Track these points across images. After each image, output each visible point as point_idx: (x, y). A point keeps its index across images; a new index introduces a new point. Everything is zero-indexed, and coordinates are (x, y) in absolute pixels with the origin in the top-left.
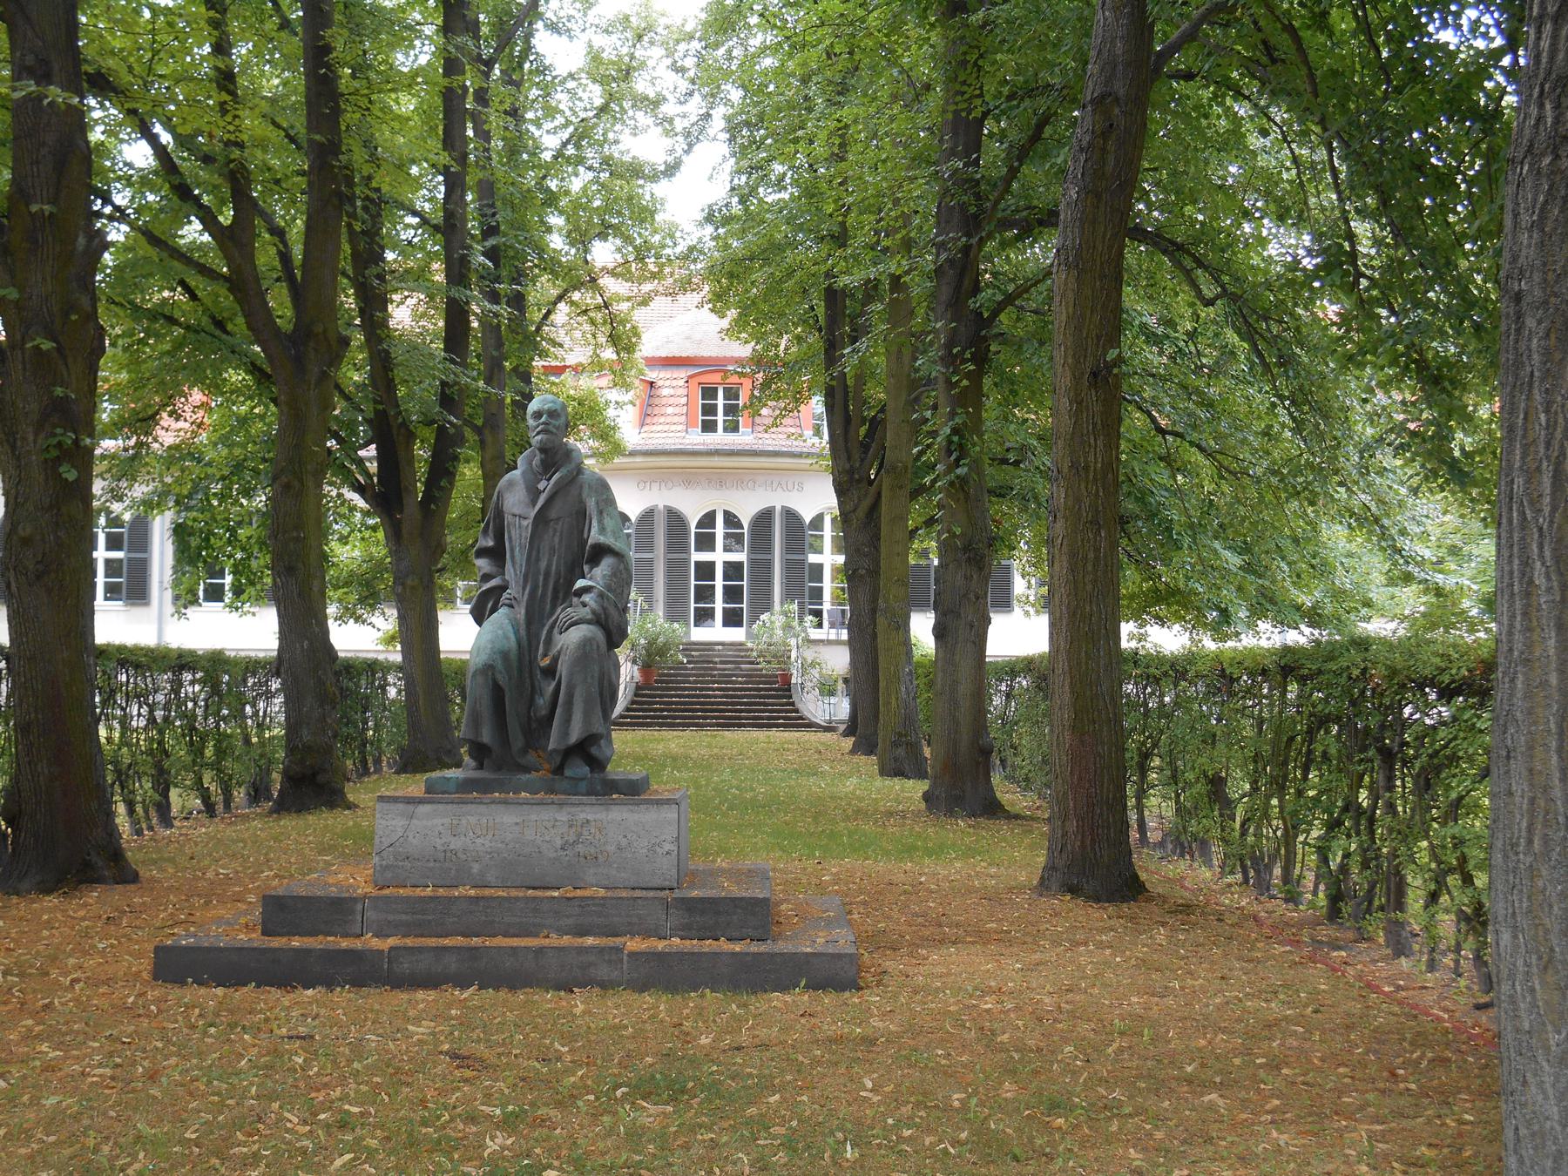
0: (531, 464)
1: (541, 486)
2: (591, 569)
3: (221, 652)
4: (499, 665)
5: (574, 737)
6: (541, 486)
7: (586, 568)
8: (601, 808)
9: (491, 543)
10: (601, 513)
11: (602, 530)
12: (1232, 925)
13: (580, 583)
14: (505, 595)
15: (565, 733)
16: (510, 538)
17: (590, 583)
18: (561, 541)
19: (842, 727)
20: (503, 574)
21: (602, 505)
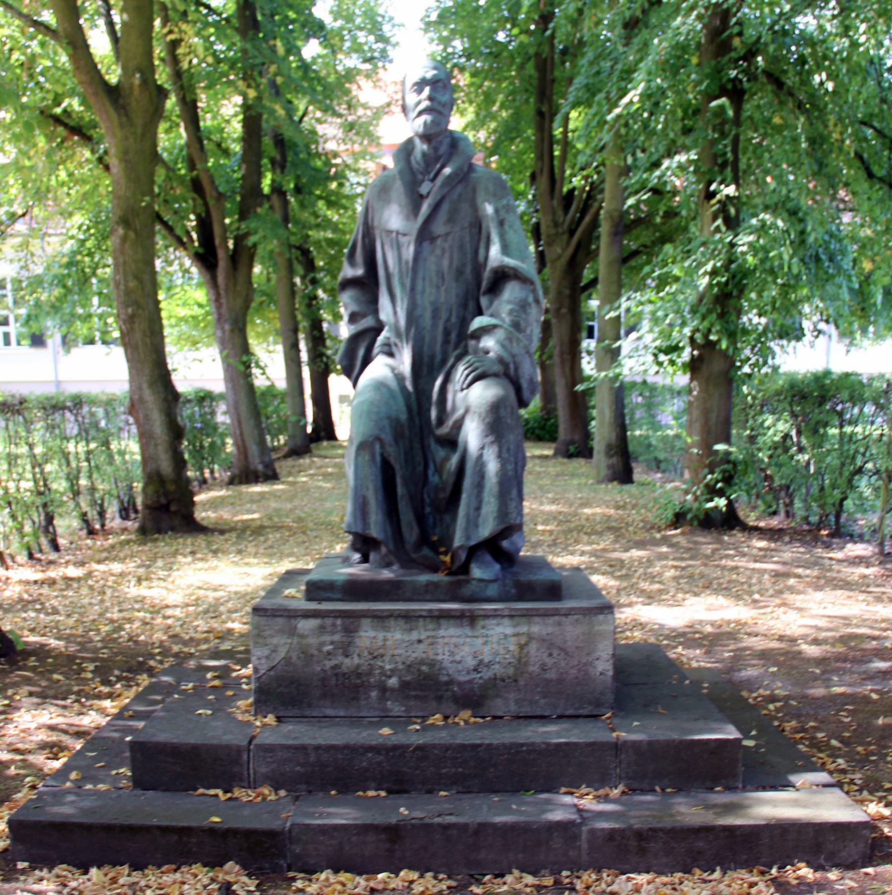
0: (408, 162)
1: (424, 189)
2: (491, 303)
3: (827, 373)
4: (387, 437)
5: (486, 530)
6: (424, 189)
7: (484, 301)
8: (523, 619)
9: (360, 272)
10: (501, 223)
11: (505, 249)
12: (853, 268)
13: (478, 322)
14: (381, 339)
15: (473, 523)
16: (386, 268)
17: (493, 321)
18: (451, 263)
19: (610, 697)
20: (376, 312)
21: (503, 213)
